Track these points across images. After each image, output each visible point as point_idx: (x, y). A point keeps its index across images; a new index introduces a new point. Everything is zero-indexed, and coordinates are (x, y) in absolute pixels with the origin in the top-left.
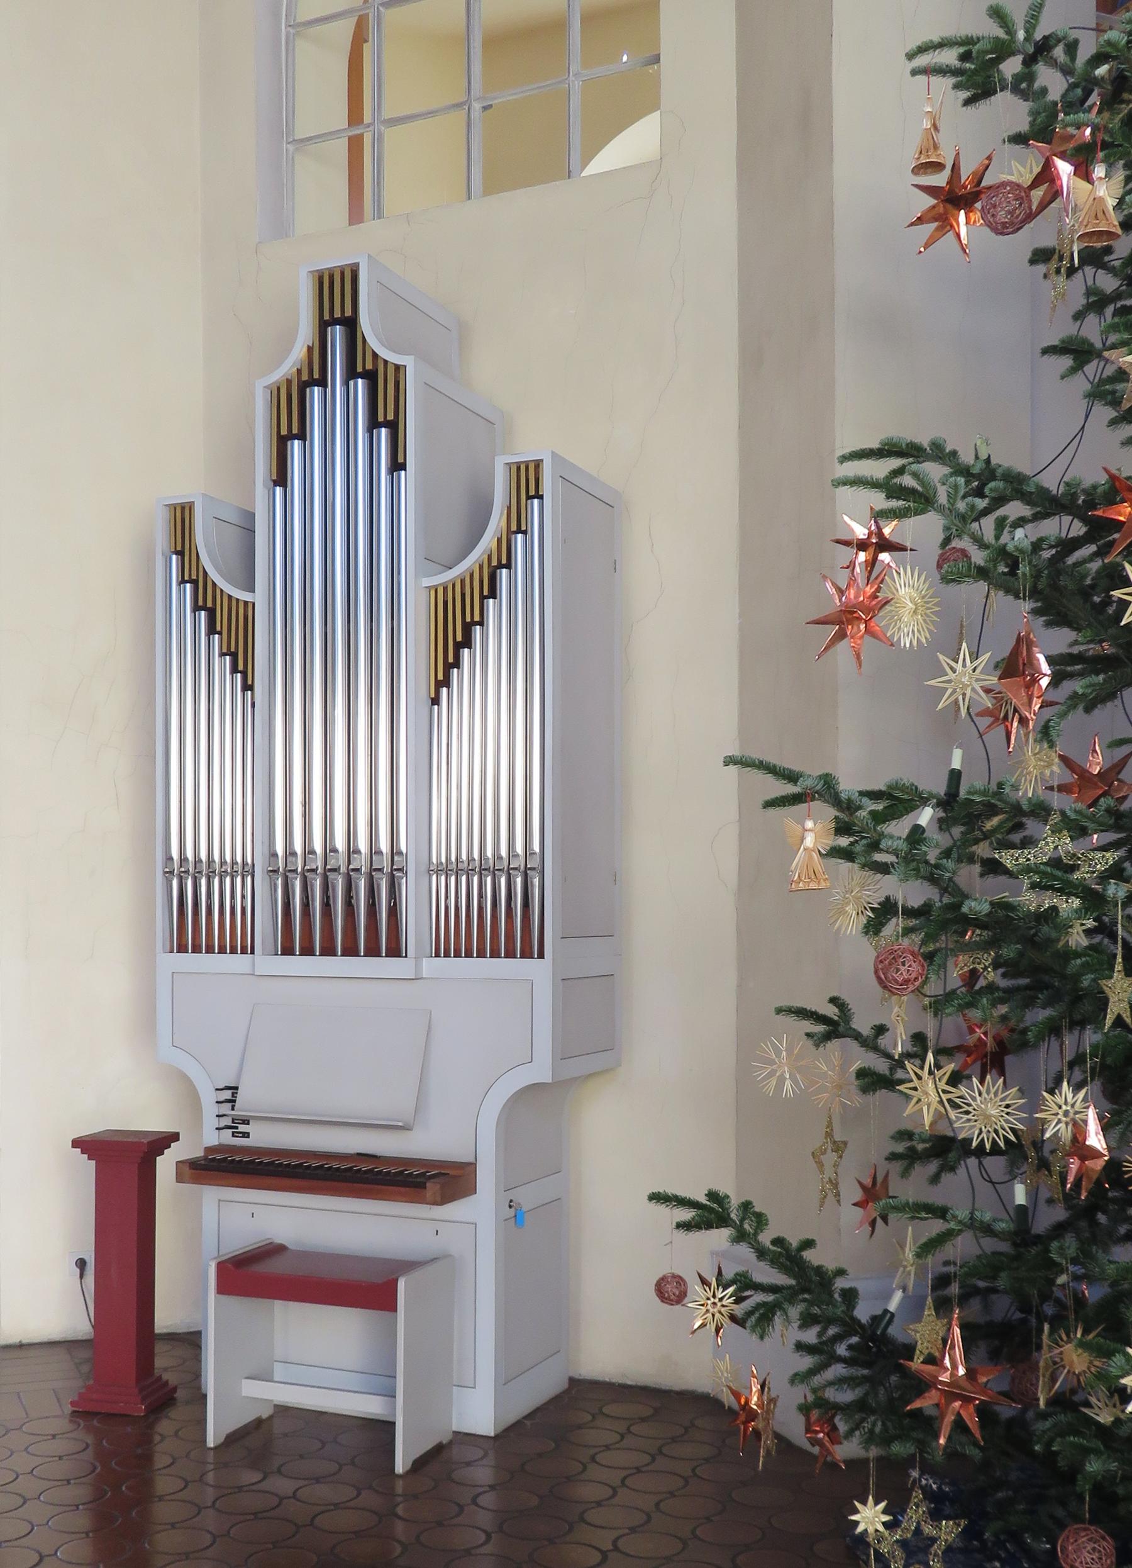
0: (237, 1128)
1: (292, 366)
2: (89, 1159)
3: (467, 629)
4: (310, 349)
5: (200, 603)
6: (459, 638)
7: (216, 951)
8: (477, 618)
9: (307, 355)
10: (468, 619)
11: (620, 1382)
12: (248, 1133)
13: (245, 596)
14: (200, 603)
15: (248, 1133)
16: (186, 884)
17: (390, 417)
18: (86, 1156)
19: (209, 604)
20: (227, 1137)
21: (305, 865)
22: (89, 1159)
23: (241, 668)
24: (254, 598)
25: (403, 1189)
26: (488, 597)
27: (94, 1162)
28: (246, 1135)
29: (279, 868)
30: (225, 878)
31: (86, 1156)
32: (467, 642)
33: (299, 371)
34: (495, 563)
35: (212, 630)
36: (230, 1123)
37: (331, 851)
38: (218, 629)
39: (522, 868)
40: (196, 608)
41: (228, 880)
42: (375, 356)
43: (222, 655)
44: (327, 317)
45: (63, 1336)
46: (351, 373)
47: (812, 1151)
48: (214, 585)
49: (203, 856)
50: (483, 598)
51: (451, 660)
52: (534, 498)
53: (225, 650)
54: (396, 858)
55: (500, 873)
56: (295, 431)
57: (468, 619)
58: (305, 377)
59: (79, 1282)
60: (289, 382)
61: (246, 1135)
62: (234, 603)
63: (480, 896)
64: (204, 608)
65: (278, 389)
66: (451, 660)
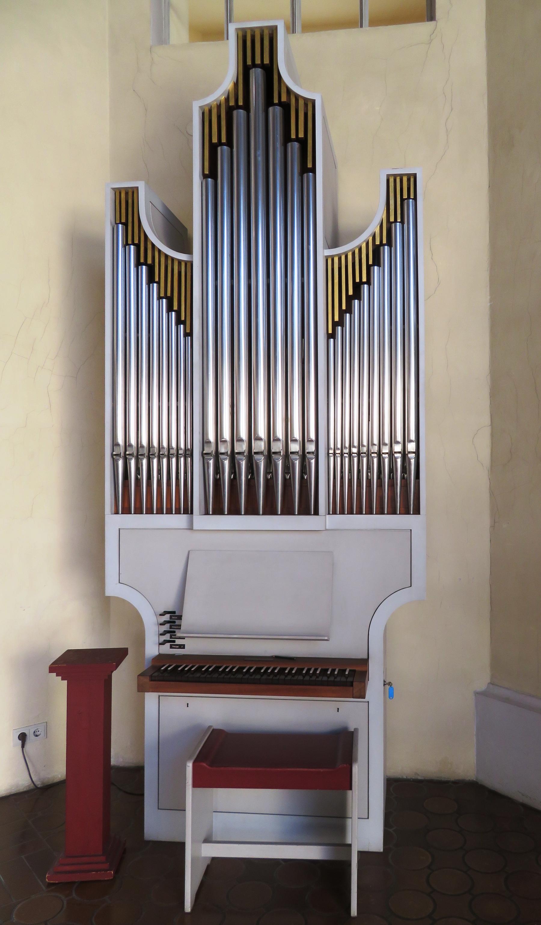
0: (174, 641)
1: (215, 100)
2: (62, 679)
3: (357, 287)
4: (236, 85)
5: (142, 260)
6: (351, 293)
7: (174, 513)
8: (364, 279)
9: (233, 87)
10: (358, 280)
11: (414, 778)
12: (184, 645)
13: (183, 257)
14: (142, 260)
15: (184, 645)
16: (153, 462)
17: (301, 135)
18: (60, 678)
19: (149, 261)
20: (166, 649)
21: (113, 451)
22: (62, 679)
23: (175, 308)
24: (192, 258)
25: (334, 688)
26: (374, 265)
27: (66, 681)
28: (182, 647)
29: (121, 453)
30: (162, 459)
31: (60, 678)
32: (357, 294)
33: (227, 99)
34: (378, 242)
35: (151, 280)
36: (169, 639)
37: (274, 440)
38: (157, 279)
39: (135, 454)
40: (138, 264)
41: (165, 461)
42: (289, 91)
43: (159, 298)
44: (249, 62)
45: (9, 791)
46: (269, 102)
47: (189, 550)
48: (153, 246)
49: (145, 442)
50: (369, 267)
51: (344, 307)
52: (164, 298)
53: (162, 295)
54: (140, 449)
55: (130, 457)
56: (224, 140)
57: (358, 280)
58: (232, 103)
59: (21, 751)
60: (219, 107)
61: (182, 647)
62: (170, 262)
63: (342, 472)
64: (145, 263)
65: (210, 111)
66: (344, 307)
